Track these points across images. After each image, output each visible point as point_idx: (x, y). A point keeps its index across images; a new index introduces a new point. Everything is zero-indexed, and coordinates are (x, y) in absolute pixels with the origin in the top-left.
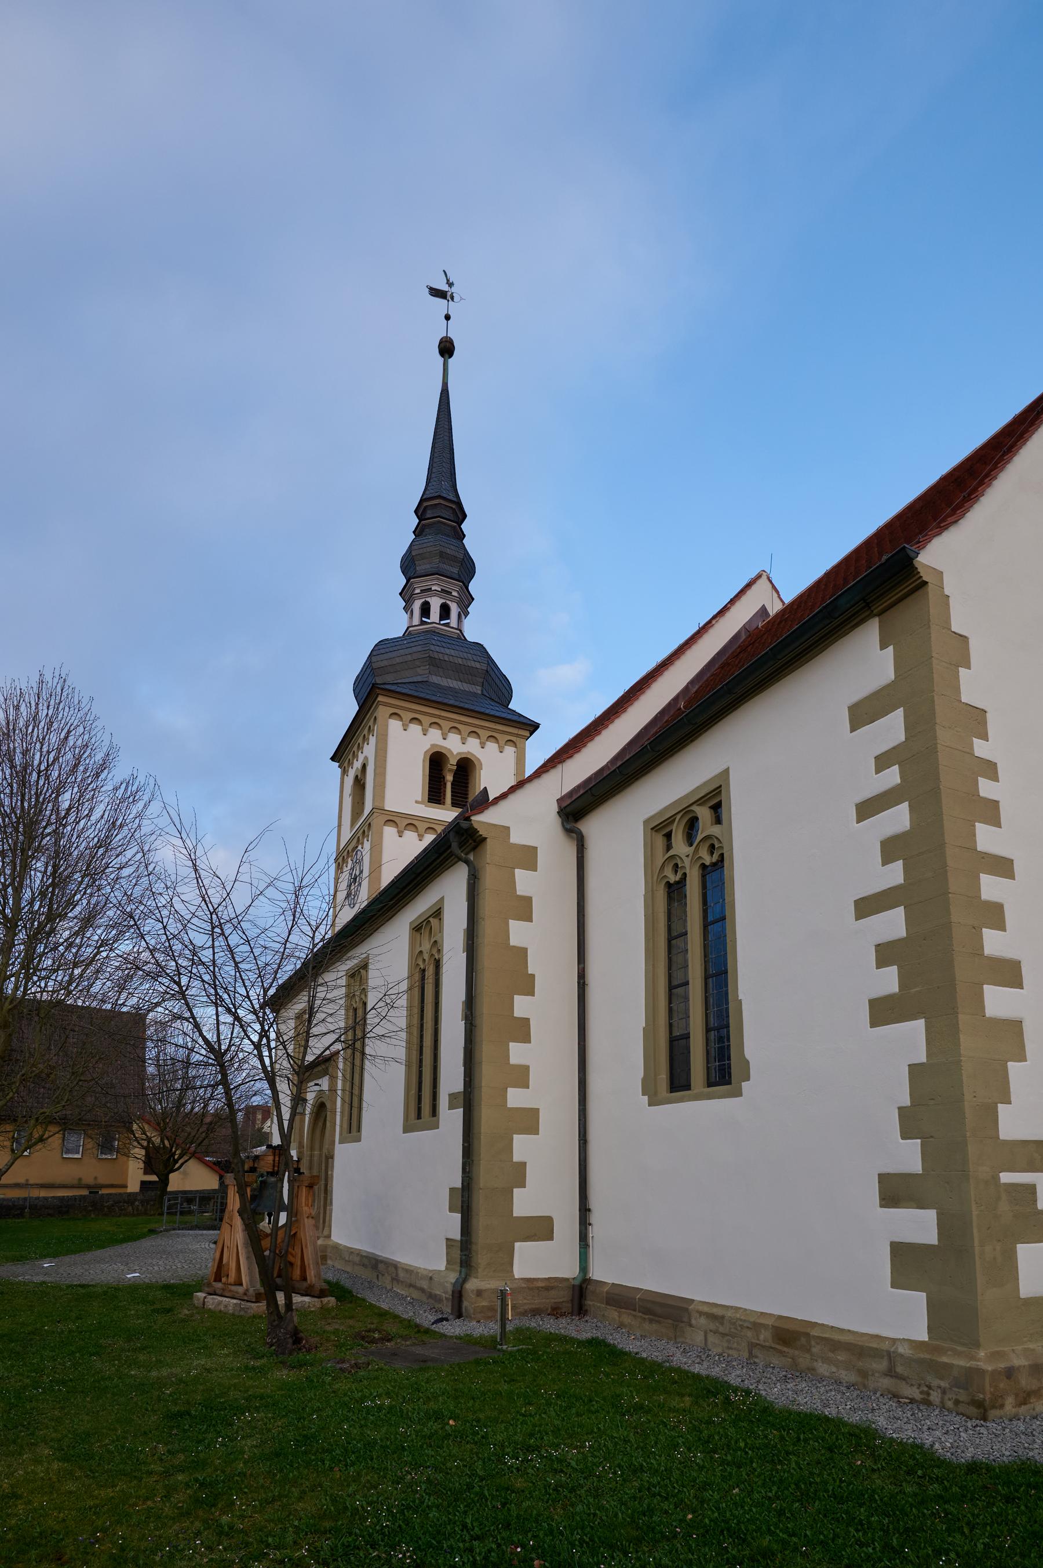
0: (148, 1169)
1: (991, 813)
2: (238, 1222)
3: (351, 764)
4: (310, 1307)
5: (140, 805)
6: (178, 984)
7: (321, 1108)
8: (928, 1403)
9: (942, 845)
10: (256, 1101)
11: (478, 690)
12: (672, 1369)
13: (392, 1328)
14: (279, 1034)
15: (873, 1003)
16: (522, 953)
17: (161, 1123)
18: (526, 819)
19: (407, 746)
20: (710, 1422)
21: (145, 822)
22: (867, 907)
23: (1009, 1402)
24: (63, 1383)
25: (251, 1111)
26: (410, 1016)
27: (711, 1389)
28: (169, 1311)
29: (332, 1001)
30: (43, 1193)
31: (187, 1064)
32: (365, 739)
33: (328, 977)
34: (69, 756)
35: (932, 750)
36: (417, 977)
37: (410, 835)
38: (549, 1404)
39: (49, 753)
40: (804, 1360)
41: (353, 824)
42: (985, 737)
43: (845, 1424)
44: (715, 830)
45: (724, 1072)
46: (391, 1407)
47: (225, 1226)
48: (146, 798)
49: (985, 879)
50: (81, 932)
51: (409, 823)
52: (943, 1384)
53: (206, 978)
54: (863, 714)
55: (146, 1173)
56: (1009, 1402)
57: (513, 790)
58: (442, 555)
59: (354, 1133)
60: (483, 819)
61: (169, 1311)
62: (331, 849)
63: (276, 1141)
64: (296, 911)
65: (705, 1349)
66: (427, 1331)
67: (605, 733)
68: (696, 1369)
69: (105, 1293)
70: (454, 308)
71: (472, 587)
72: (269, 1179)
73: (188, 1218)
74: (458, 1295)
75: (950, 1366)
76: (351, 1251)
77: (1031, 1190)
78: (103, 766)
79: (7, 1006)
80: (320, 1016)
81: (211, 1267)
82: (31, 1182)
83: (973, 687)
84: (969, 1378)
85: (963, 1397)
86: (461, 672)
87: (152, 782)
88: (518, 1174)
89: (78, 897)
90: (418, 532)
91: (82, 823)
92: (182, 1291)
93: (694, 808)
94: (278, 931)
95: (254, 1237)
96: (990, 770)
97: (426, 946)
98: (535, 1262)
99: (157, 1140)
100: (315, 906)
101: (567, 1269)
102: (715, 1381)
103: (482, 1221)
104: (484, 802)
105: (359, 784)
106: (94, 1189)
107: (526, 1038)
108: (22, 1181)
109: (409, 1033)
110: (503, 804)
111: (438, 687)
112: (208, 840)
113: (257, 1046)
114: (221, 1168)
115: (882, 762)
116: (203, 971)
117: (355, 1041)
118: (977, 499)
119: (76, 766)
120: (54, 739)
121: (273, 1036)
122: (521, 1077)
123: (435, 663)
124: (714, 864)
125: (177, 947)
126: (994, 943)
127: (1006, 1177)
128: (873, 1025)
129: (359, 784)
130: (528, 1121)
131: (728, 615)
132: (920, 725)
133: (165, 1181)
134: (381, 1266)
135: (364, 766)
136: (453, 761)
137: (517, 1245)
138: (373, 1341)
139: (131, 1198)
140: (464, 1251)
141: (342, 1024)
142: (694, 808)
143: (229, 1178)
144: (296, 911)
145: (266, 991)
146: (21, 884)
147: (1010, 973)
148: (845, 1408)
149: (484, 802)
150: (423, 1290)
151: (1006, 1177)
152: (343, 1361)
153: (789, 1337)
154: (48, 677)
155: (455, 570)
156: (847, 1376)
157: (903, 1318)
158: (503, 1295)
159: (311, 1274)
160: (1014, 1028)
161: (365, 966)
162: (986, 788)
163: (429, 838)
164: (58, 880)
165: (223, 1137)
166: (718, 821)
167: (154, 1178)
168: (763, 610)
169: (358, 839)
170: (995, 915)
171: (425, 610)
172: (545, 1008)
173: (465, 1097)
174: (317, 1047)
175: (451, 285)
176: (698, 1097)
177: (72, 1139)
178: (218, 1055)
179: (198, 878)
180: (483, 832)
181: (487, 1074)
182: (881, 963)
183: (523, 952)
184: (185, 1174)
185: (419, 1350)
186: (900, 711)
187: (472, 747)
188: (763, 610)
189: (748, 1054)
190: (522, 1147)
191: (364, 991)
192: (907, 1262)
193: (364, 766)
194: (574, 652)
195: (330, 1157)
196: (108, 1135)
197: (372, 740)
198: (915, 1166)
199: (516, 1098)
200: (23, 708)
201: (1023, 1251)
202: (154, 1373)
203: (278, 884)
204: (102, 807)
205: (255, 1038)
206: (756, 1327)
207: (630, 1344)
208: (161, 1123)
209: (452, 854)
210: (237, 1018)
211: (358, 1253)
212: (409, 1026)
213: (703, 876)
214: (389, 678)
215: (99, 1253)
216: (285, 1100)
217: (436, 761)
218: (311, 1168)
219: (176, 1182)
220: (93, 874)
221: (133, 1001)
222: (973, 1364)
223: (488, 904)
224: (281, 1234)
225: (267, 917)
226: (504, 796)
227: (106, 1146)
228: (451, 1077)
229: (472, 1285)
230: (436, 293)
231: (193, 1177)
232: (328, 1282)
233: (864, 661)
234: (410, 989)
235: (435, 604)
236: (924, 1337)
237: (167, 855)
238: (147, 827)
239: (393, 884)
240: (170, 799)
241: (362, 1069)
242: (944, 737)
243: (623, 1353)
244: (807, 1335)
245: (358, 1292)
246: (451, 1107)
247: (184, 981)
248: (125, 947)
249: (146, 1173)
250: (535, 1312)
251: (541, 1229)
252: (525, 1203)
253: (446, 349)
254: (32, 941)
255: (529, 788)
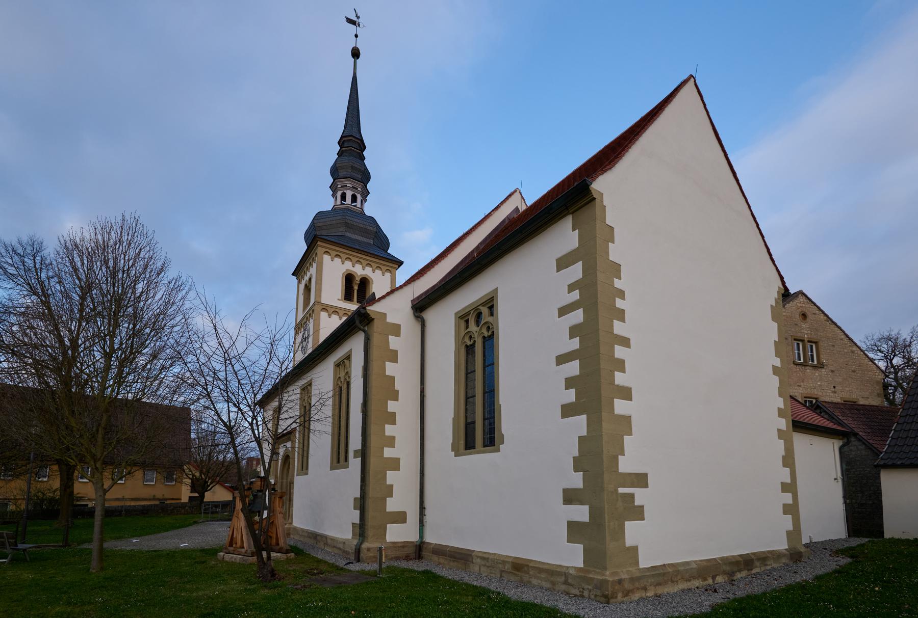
0: (193, 489)
1: (621, 315)
2: (241, 516)
3: (303, 277)
4: (280, 560)
5: (184, 292)
6: (206, 390)
7: (287, 458)
8: (582, 596)
9: (598, 330)
10: (253, 454)
11: (371, 242)
12: (463, 584)
13: (323, 568)
14: (263, 419)
15: (563, 407)
16: (392, 379)
17: (199, 465)
18: (395, 310)
19: (333, 270)
20: (480, 608)
21: (186, 302)
22: (562, 359)
23: (620, 595)
24: (142, 601)
25: (250, 460)
26: (334, 410)
27: (481, 592)
28: (203, 562)
29: (291, 401)
30: (133, 503)
31: (215, 433)
32: (311, 265)
33: (290, 388)
34: (141, 263)
35: (595, 284)
36: (338, 389)
37: (335, 317)
38: (402, 602)
39: (129, 260)
40: (526, 578)
41: (304, 310)
42: (619, 278)
43: (544, 607)
44: (490, 319)
45: (492, 440)
46: (322, 606)
47: (235, 519)
48: (187, 289)
49: (617, 348)
50: (151, 361)
51: (335, 311)
52: (590, 587)
53: (222, 387)
54: (563, 263)
55: (192, 492)
56: (620, 595)
57: (388, 294)
58: (352, 167)
59: (304, 470)
60: (373, 309)
61: (203, 562)
62: (293, 325)
63: (263, 474)
64: (272, 353)
65: (480, 574)
66: (342, 569)
67: (437, 267)
68: (475, 583)
69: (168, 554)
70: (360, 31)
71: (369, 186)
72: (259, 493)
73: (215, 515)
74: (358, 551)
75: (592, 579)
76: (303, 530)
77: (632, 496)
78: (162, 270)
79: (107, 400)
80: (285, 409)
81: (227, 539)
82: (126, 497)
83: (615, 253)
84: (602, 584)
85: (599, 593)
86: (364, 232)
87: (190, 280)
88: (389, 491)
89: (148, 342)
90: (340, 154)
91: (149, 301)
92: (212, 552)
93: (480, 307)
94: (262, 363)
95: (250, 524)
96: (621, 294)
97: (342, 375)
98: (396, 534)
99: (197, 474)
100: (282, 351)
101: (414, 537)
102: (484, 588)
103: (370, 514)
104: (373, 300)
105: (308, 288)
106: (162, 501)
107: (394, 422)
108: (120, 497)
109: (333, 419)
110: (383, 301)
111: (350, 238)
112: (222, 314)
113: (251, 424)
114: (232, 489)
115: (571, 288)
116: (220, 383)
117: (305, 421)
118: (621, 158)
119: (145, 269)
120: (132, 253)
121: (259, 419)
122: (391, 442)
123: (348, 226)
124: (489, 337)
125: (206, 371)
126: (620, 379)
127: (621, 490)
128: (562, 417)
129: (308, 288)
130: (395, 464)
131: (500, 210)
132: (590, 271)
133: (202, 496)
134: (319, 538)
135: (310, 279)
136: (358, 279)
137: (388, 526)
138: (314, 574)
139: (183, 505)
140: (361, 529)
141: (298, 413)
142: (480, 307)
143: (237, 493)
144: (272, 353)
145: (255, 395)
146: (114, 335)
147: (626, 394)
148: (543, 599)
149: (373, 300)
150: (340, 549)
151: (621, 490)
152: (297, 585)
153: (519, 567)
154: (127, 217)
155: (360, 177)
156: (546, 585)
157: (572, 557)
158: (380, 550)
159: (281, 542)
160: (627, 419)
161: (310, 385)
162: (619, 303)
163: (344, 318)
164: (135, 333)
165: (235, 473)
166: (492, 315)
167: (197, 495)
168: (517, 209)
169: (306, 319)
170: (620, 365)
171: (344, 197)
172: (403, 407)
173: (365, 457)
174: (283, 426)
175: (358, 18)
176: (478, 453)
177: (149, 474)
178: (231, 429)
179: (217, 333)
180: (372, 315)
181: (373, 441)
182: (567, 387)
183: (393, 378)
184: (214, 492)
185: (337, 578)
186: (581, 263)
187: (368, 272)
188: (517, 209)
189: (503, 431)
190: (391, 477)
191: (310, 397)
192: (575, 530)
193: (310, 279)
194: (422, 224)
195: (292, 483)
196: (170, 471)
197: (315, 265)
198: (580, 485)
199: (388, 452)
200: (113, 234)
201: (628, 524)
202: (194, 594)
203: (262, 338)
204: (161, 292)
205: (250, 420)
206: (504, 562)
207: (443, 573)
208: (199, 465)
209: (356, 327)
210: (239, 409)
211: (307, 532)
212: (333, 415)
213: (484, 343)
214: (324, 232)
215: (165, 534)
216: (267, 453)
217: (349, 278)
218: (282, 489)
219: (209, 497)
220: (158, 330)
221: (181, 399)
222: (604, 577)
223: (375, 353)
224: (264, 522)
225: (255, 356)
226: (383, 297)
227: (169, 478)
228: (355, 442)
229: (365, 545)
230: (350, 21)
231: (218, 494)
232: (291, 546)
233: (564, 237)
234: (334, 396)
235: (349, 194)
236: (582, 566)
237: (201, 322)
238: (187, 305)
239: (325, 341)
240: (201, 290)
241: (309, 437)
242: (600, 277)
243: (439, 577)
244: (528, 566)
245: (307, 552)
246: (355, 457)
247: (209, 389)
248: (176, 369)
249: (192, 492)
250: (397, 558)
251: (400, 517)
252: (392, 505)
253: (356, 54)
254: (122, 365)
255: (397, 294)
